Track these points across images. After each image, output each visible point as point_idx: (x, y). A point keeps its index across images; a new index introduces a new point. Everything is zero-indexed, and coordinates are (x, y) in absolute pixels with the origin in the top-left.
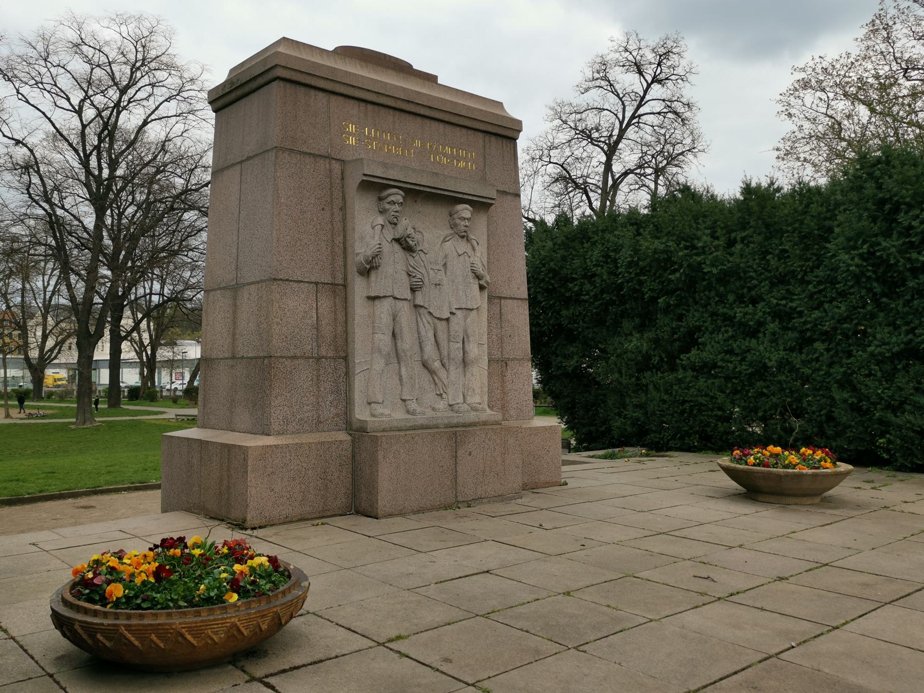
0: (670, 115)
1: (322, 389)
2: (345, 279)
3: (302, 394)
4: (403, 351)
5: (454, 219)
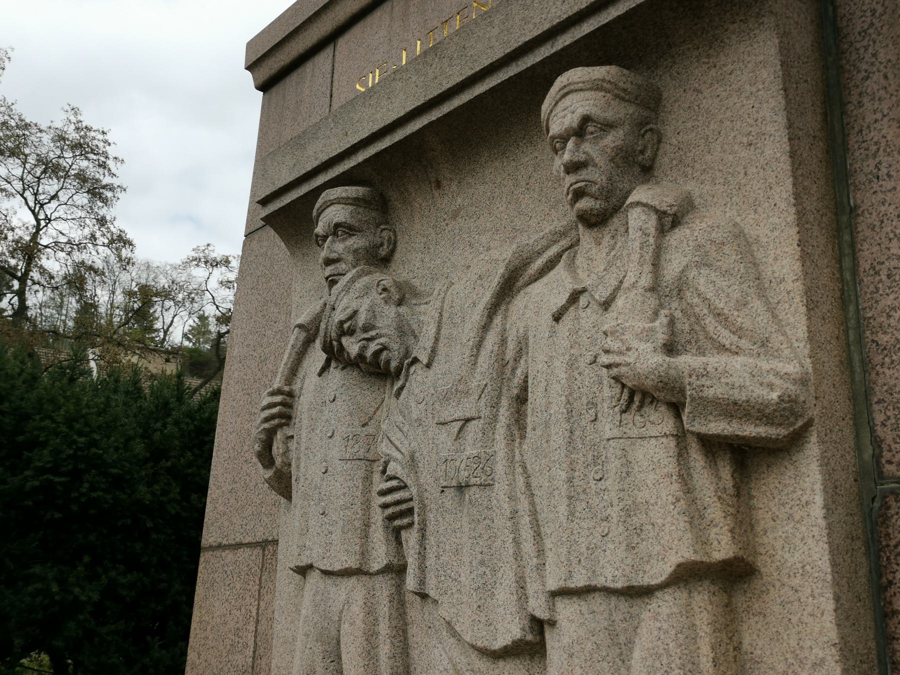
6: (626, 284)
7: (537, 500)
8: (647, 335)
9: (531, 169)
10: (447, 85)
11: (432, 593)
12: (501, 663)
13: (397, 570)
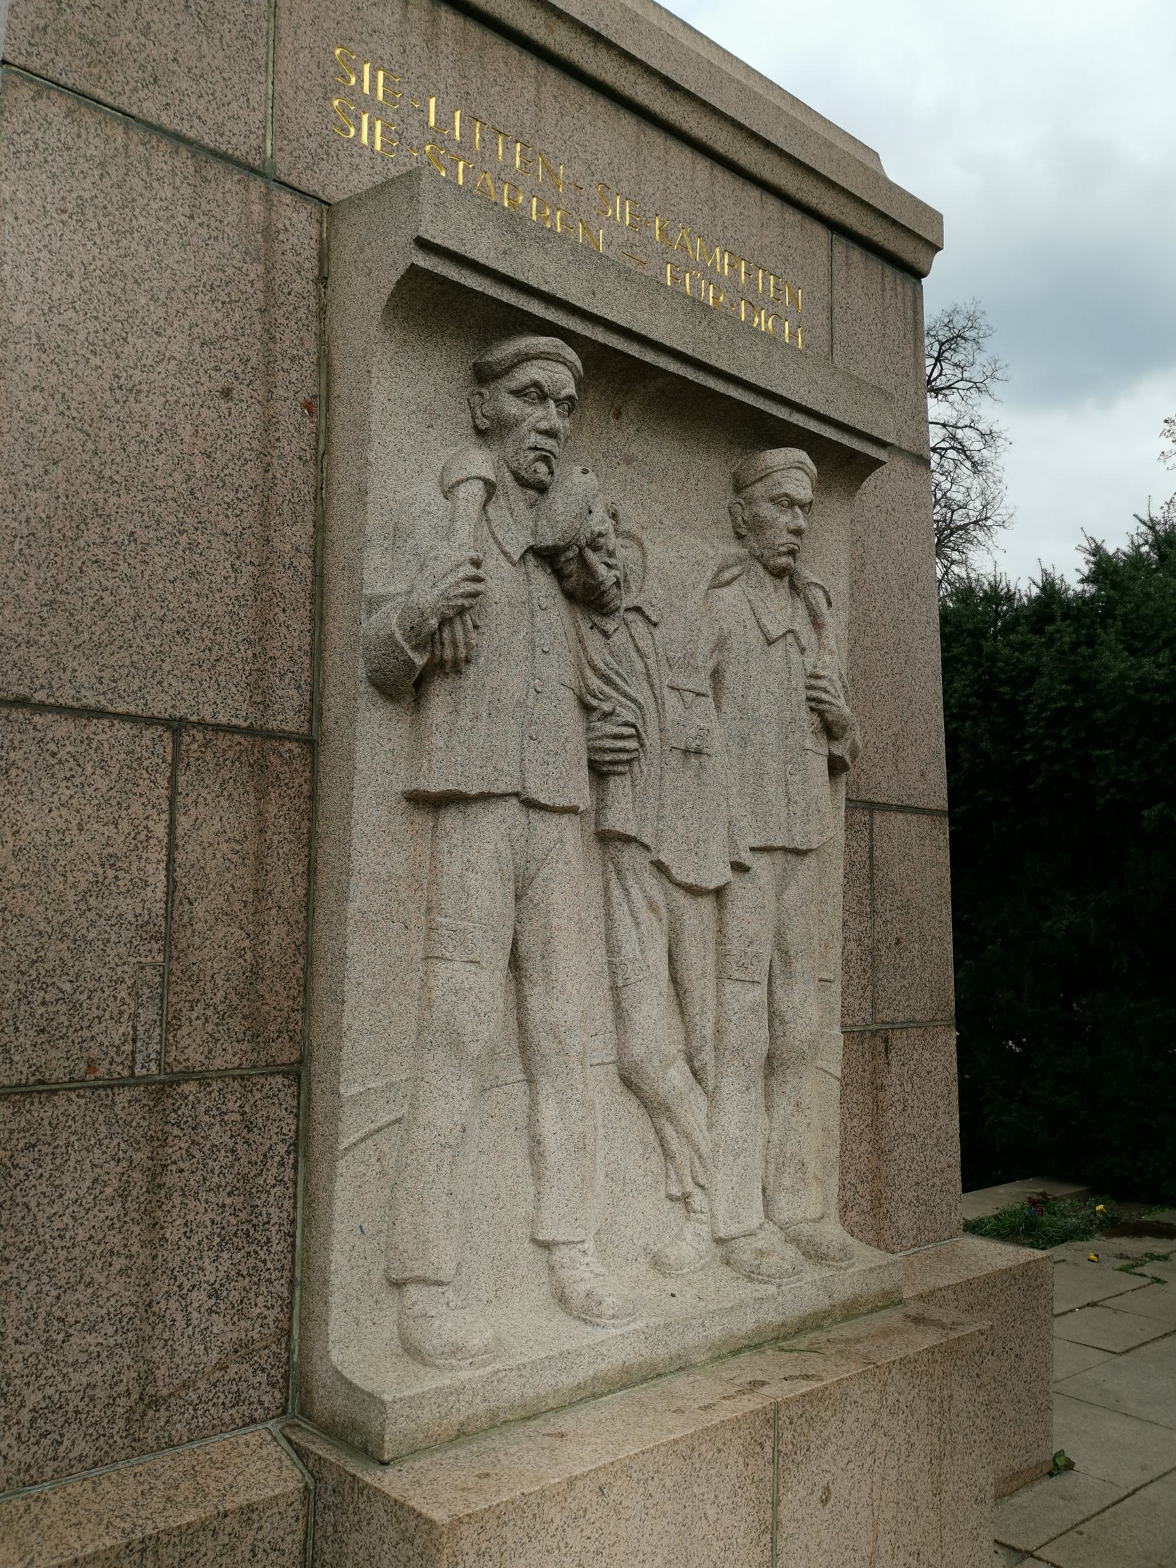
0: (951, 454)
1: (173, 1233)
2: (314, 711)
3: (62, 1276)
4: (553, 1031)
5: (750, 502)
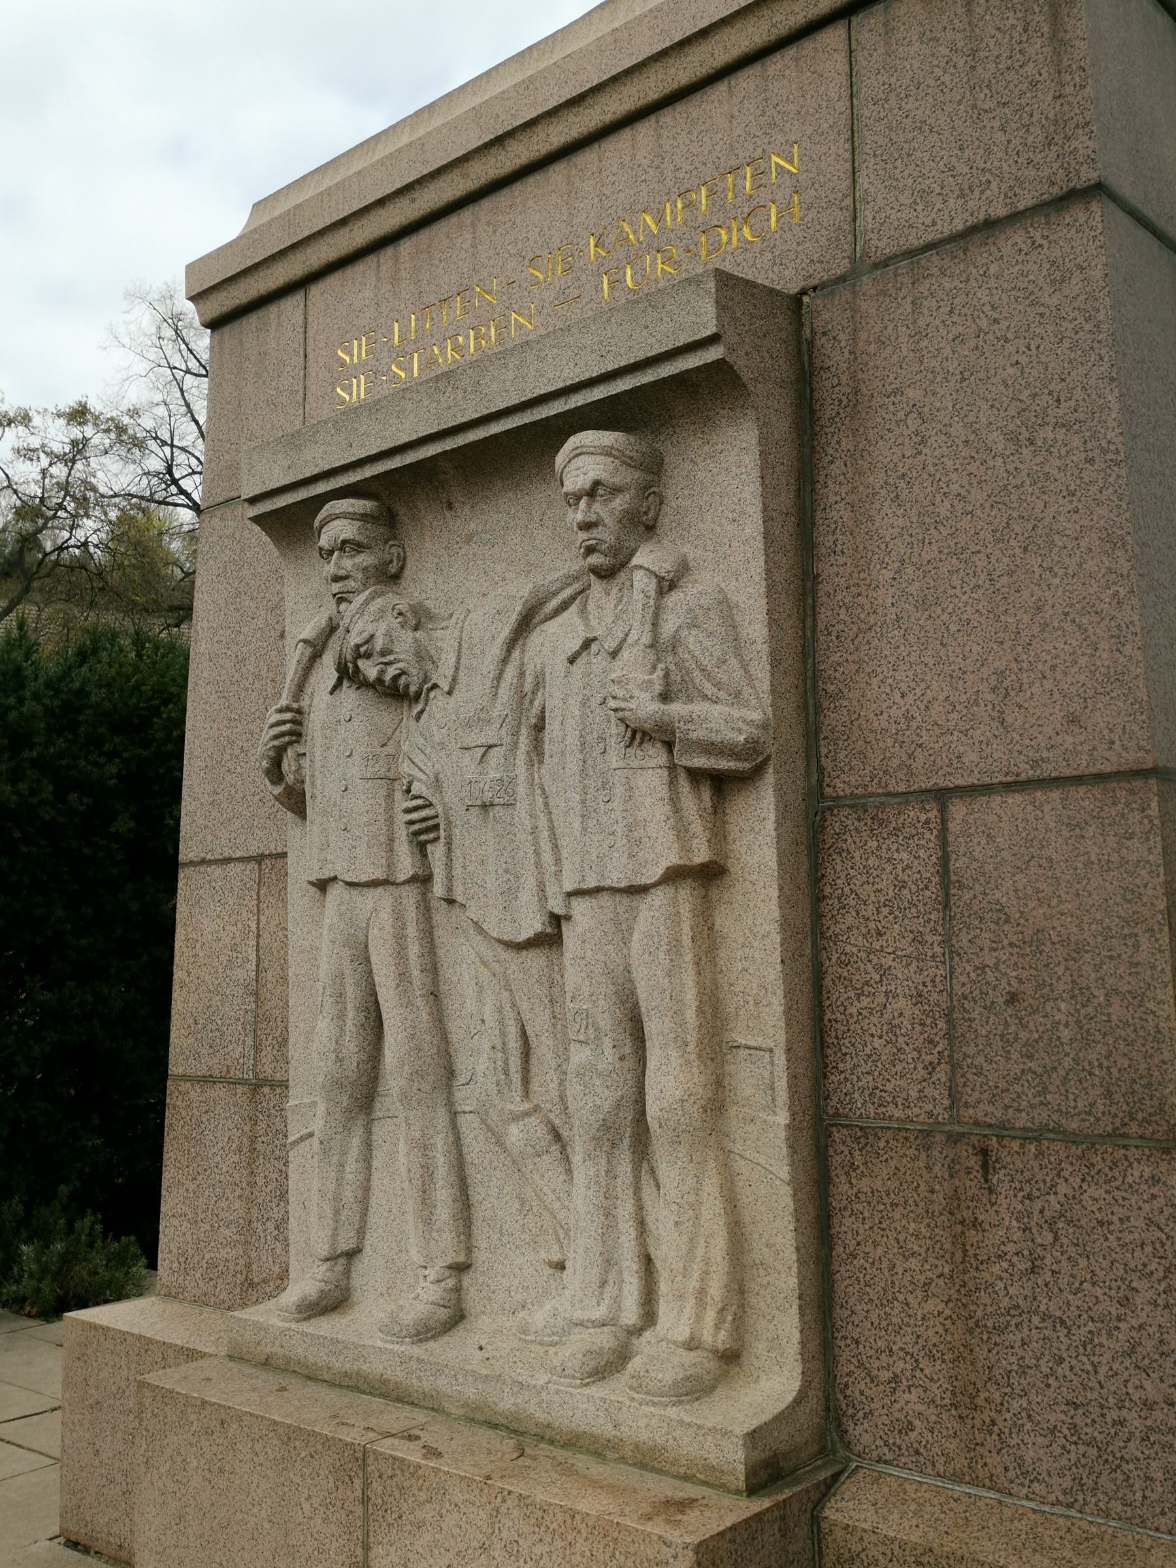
1: (260, 1181)
6: (630, 640)
7: (554, 817)
8: (647, 685)
9: (544, 506)
10: (461, 420)
11: (459, 899)
12: (524, 953)
13: (423, 880)
